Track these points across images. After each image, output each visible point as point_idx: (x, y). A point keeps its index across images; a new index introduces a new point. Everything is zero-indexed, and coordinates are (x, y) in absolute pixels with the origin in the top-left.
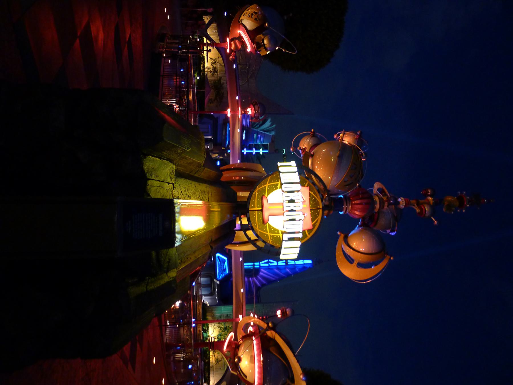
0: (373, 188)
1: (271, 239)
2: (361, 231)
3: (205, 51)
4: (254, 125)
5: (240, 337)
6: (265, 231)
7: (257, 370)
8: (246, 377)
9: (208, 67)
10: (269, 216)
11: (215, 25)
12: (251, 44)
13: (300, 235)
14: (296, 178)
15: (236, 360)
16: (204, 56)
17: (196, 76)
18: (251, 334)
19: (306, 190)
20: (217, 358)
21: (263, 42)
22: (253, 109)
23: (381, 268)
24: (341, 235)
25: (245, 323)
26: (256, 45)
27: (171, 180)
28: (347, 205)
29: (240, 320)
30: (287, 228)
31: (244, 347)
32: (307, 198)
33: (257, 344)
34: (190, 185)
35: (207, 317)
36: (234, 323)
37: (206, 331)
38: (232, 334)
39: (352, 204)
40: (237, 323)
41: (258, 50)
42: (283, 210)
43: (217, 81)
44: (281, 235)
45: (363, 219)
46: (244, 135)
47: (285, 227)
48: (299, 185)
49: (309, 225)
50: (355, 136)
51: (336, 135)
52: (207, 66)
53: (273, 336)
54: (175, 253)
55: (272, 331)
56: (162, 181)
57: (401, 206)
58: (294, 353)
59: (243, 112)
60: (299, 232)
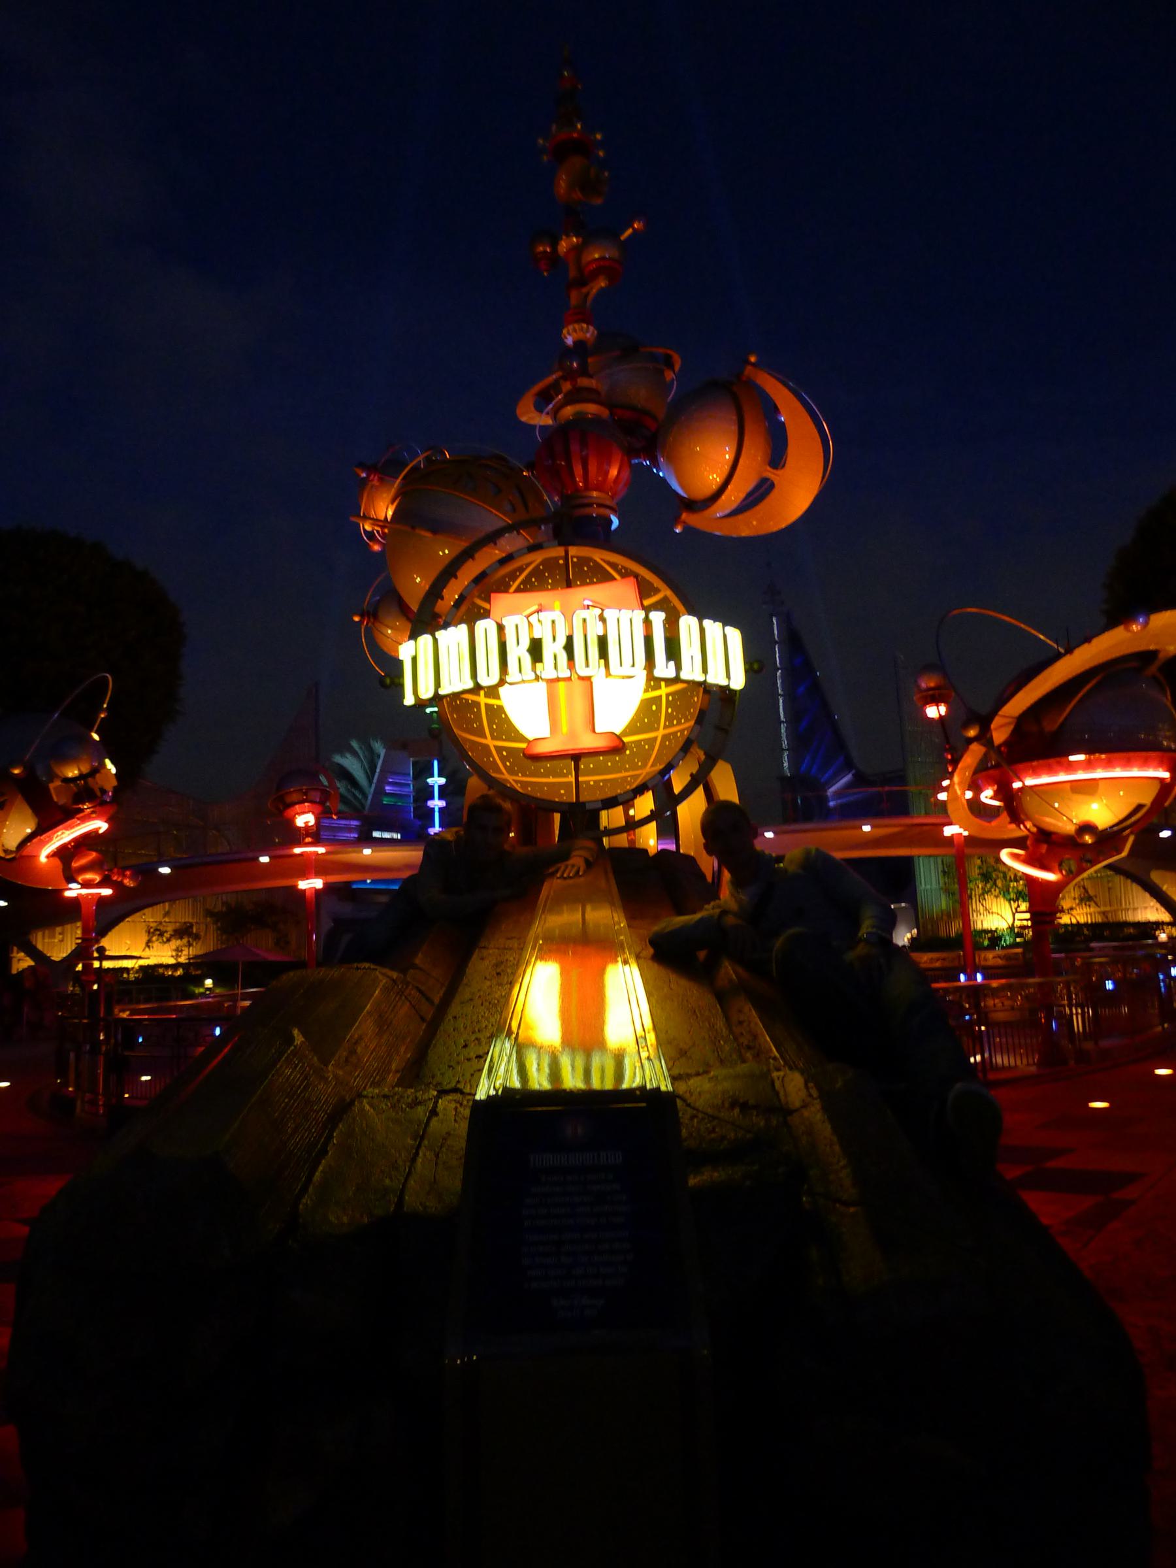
0: (536, 426)
1: (679, 723)
2: (672, 460)
3: (101, 964)
4: (357, 804)
5: (1012, 830)
6: (652, 747)
7: (1118, 773)
8: (1140, 807)
9: (174, 954)
10: (597, 731)
11: (40, 934)
12: (85, 819)
13: (658, 618)
14: (453, 637)
15: (1088, 839)
16: (141, 967)
17: (202, 990)
18: (1004, 792)
19: (500, 602)
20: (1077, 901)
21: (74, 780)
22: (298, 808)
23: (786, 392)
24: (684, 522)
25: (972, 817)
26: (84, 803)
27: (420, 1103)
28: (591, 505)
29: (961, 831)
30: (633, 666)
31: (1048, 816)
32: (532, 600)
33: (1036, 773)
34: (460, 1024)
35: (953, 934)
36: (968, 851)
37: (995, 938)
38: (1005, 855)
39: (587, 487)
40: (970, 841)
41: (99, 794)
42: (569, 679)
43: (219, 924)
44: (664, 691)
45: (631, 452)
46: (387, 835)
47: (627, 670)
48: (481, 625)
49: (625, 589)
50: (372, 487)
51: (371, 544)
52: (172, 956)
53: (1008, 724)
54: (710, 1079)
55: (993, 726)
56: (419, 1146)
57: (588, 335)
58: (1058, 656)
59: (308, 840)
60: (647, 623)
